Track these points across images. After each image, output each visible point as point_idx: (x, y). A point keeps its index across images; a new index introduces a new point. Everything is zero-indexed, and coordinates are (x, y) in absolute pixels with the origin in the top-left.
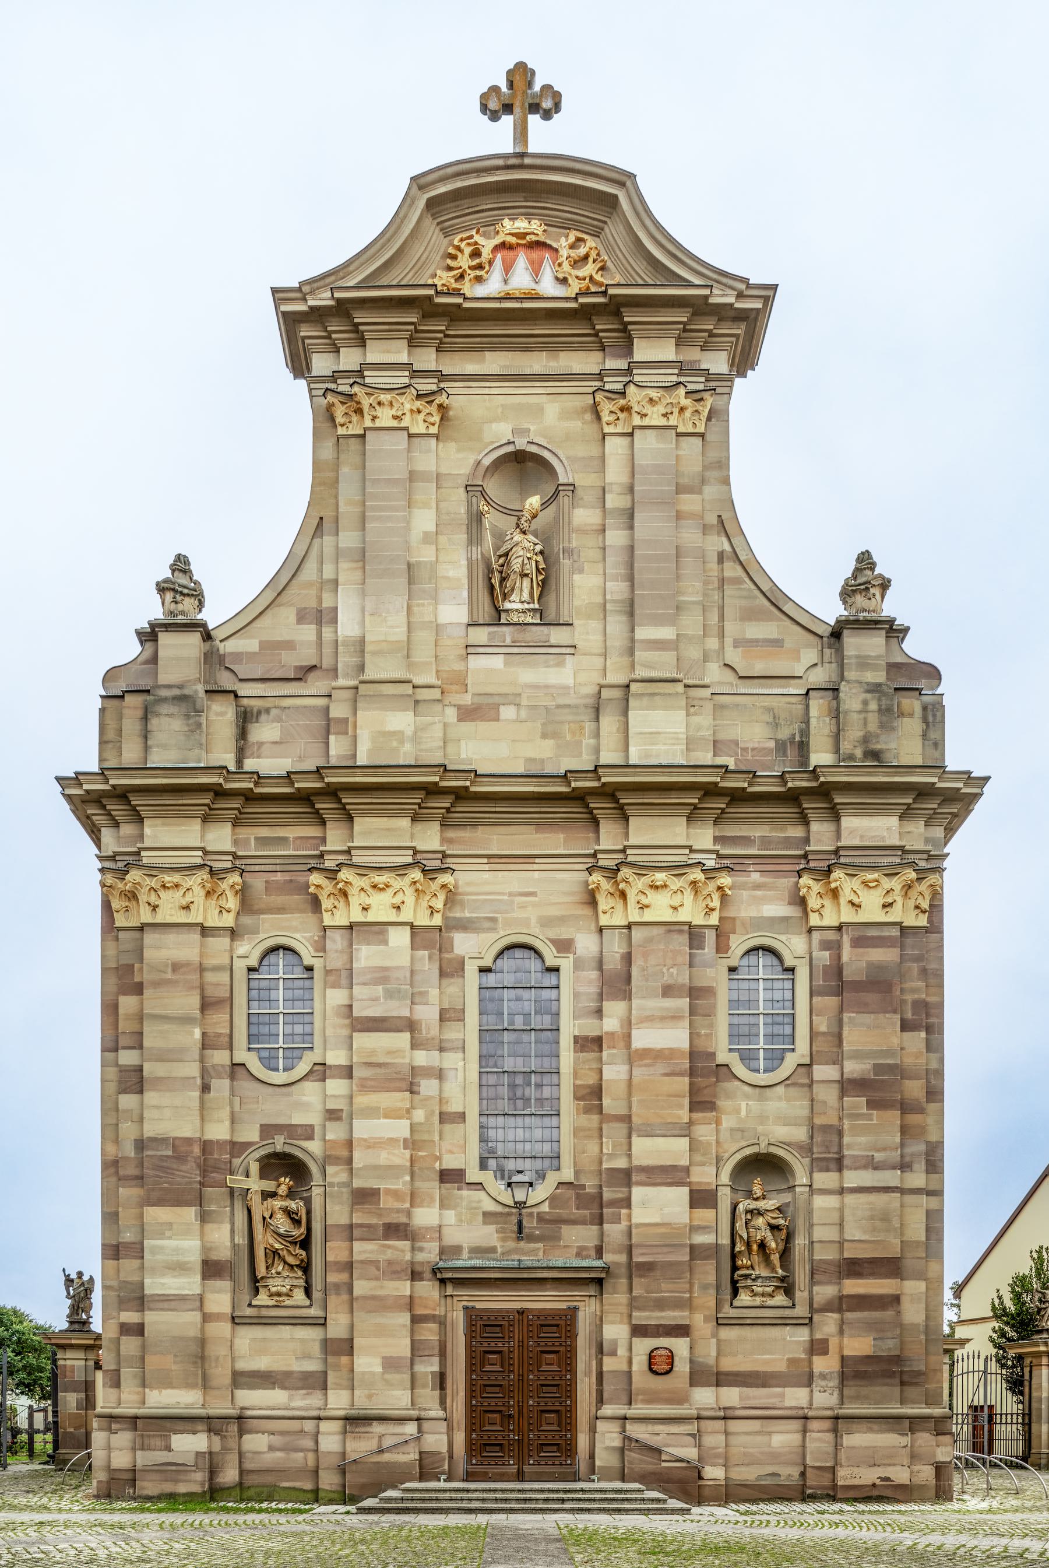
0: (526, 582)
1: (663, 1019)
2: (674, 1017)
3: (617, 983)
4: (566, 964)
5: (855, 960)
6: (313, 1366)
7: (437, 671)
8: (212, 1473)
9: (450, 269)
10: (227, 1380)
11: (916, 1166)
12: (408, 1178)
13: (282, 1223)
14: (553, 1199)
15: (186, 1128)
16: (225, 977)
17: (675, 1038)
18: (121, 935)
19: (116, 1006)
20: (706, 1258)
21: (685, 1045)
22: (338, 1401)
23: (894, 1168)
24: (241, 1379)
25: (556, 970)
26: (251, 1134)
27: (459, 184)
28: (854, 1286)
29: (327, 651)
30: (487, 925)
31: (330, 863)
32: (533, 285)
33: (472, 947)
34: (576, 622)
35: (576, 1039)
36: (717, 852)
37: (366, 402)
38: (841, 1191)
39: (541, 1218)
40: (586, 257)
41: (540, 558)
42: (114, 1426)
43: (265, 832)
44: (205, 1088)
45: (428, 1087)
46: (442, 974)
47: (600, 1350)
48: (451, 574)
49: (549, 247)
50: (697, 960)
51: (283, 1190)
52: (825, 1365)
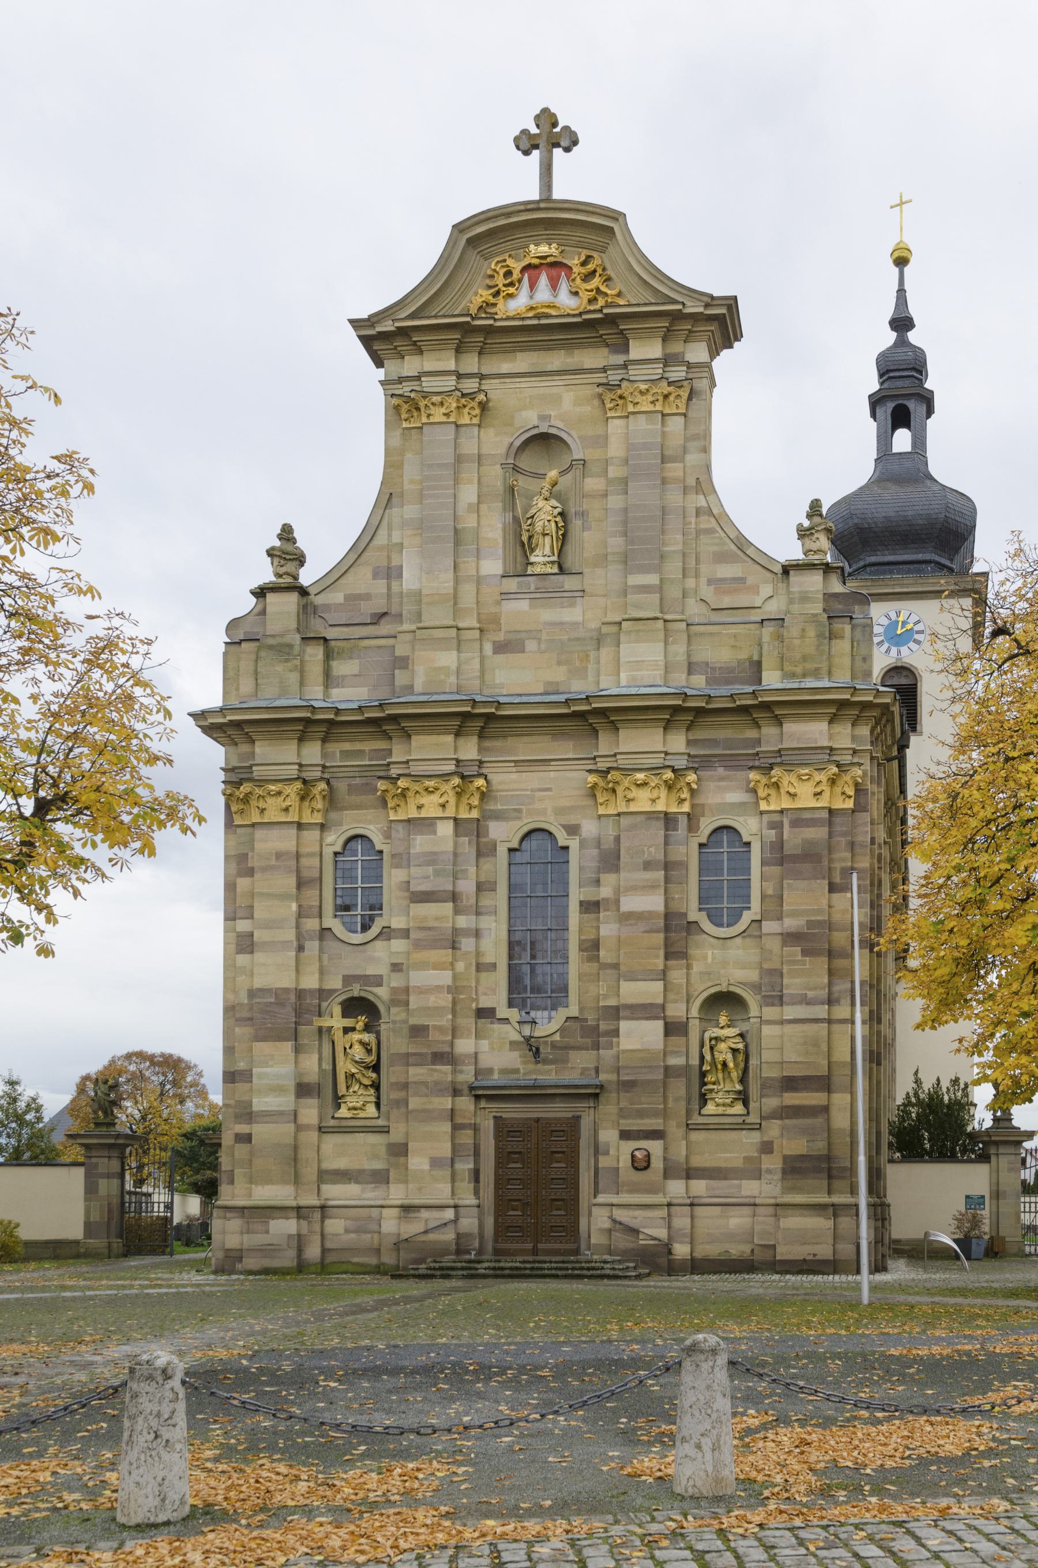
0: (548, 539)
1: (644, 888)
2: (652, 887)
3: (610, 860)
4: (574, 844)
5: (794, 838)
6: (378, 1165)
7: (479, 614)
8: (300, 1251)
9: (490, 287)
10: (314, 1177)
11: (842, 1001)
12: (450, 1017)
13: (358, 1053)
14: (562, 1030)
15: (286, 981)
16: (316, 862)
17: (654, 903)
18: (239, 830)
19: (234, 885)
20: (678, 1076)
21: (661, 908)
22: (397, 1194)
23: (823, 1003)
24: (325, 1176)
25: (566, 848)
26: (335, 983)
27: (491, 225)
28: (793, 1099)
29: (395, 600)
30: (515, 814)
31: (394, 772)
32: (552, 299)
33: (503, 833)
34: (586, 571)
35: (581, 902)
36: (689, 755)
37: (422, 404)
38: (782, 1022)
39: (554, 1046)
40: (595, 271)
41: (558, 519)
42: (228, 1215)
43: (347, 746)
44: (301, 948)
45: (467, 944)
46: (479, 854)
47: (597, 1152)
48: (490, 535)
49: (565, 265)
50: (672, 840)
51: (360, 1026)
52: (772, 1163)
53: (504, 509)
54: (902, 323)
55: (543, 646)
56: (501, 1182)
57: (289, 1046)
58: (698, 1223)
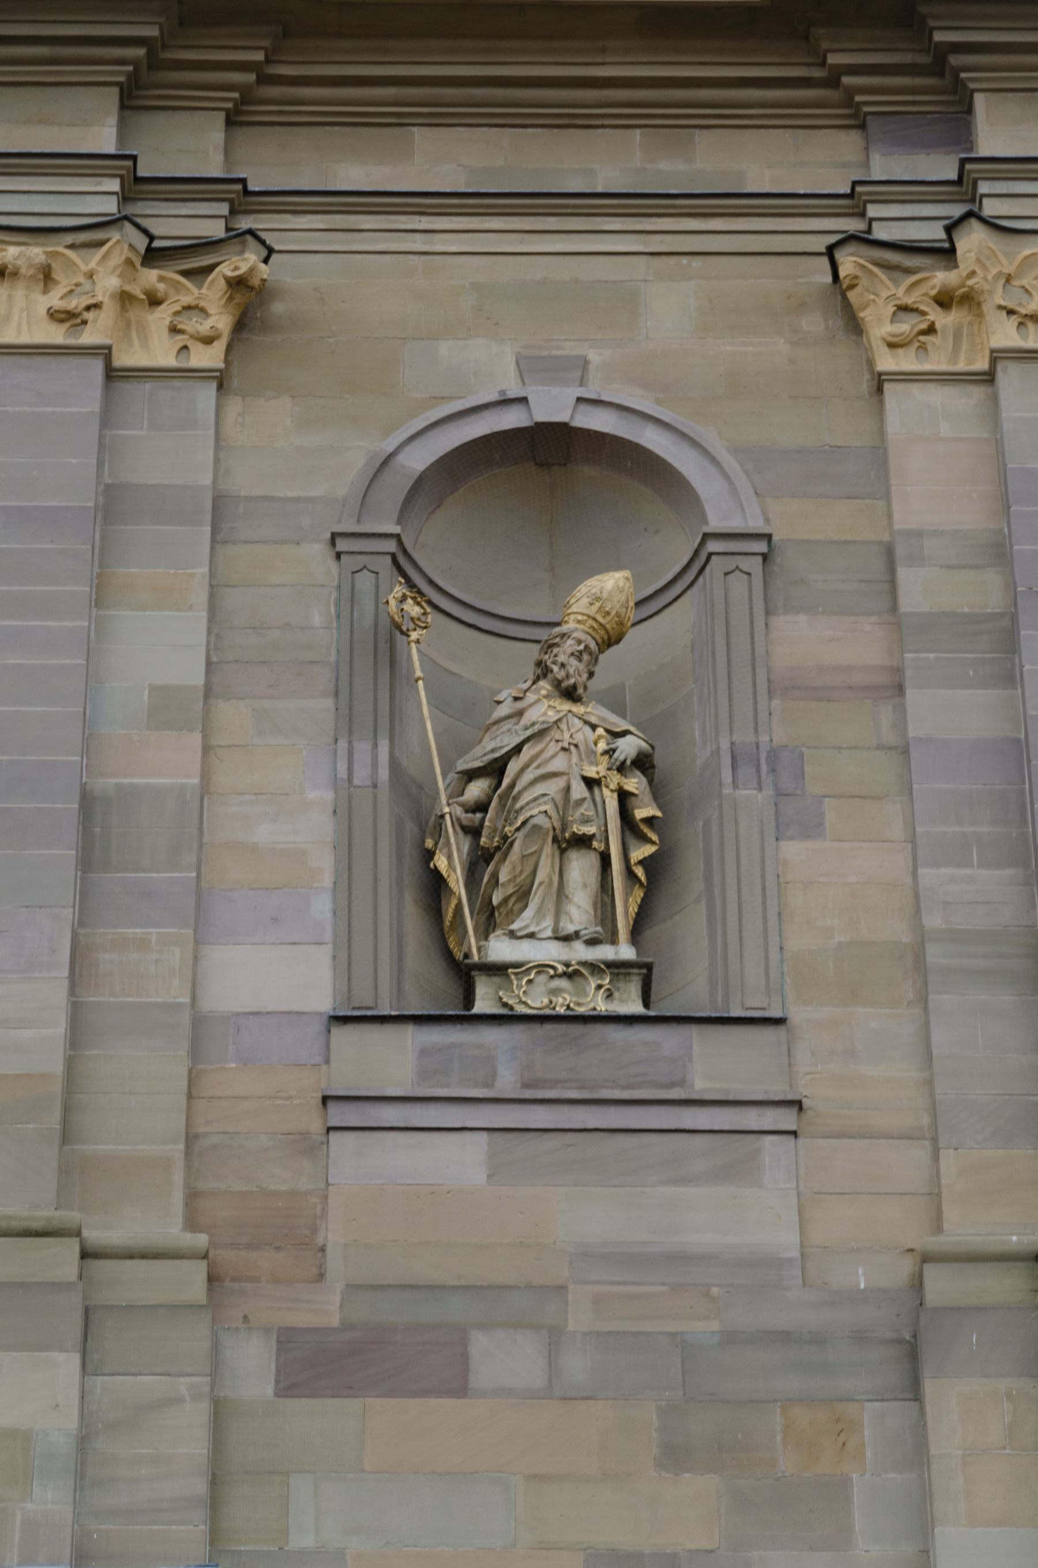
0: (581, 868)
7: (192, 1196)
53: (347, 723)
55: (577, 1366)
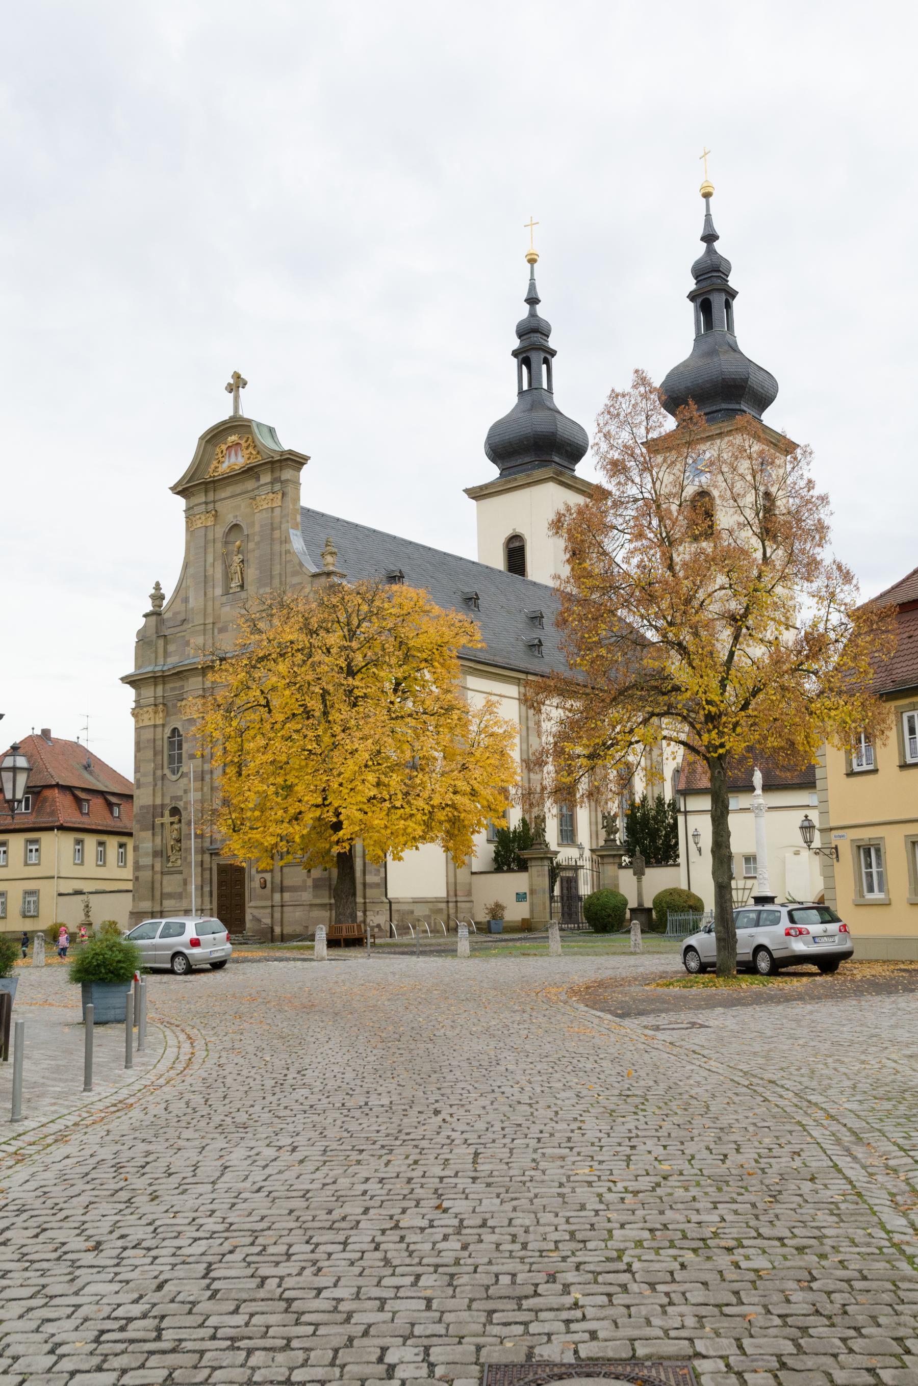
26: (167, 801)
44: (155, 785)
54: (710, 238)
56: (220, 896)
57: (150, 832)
58: (285, 915)
